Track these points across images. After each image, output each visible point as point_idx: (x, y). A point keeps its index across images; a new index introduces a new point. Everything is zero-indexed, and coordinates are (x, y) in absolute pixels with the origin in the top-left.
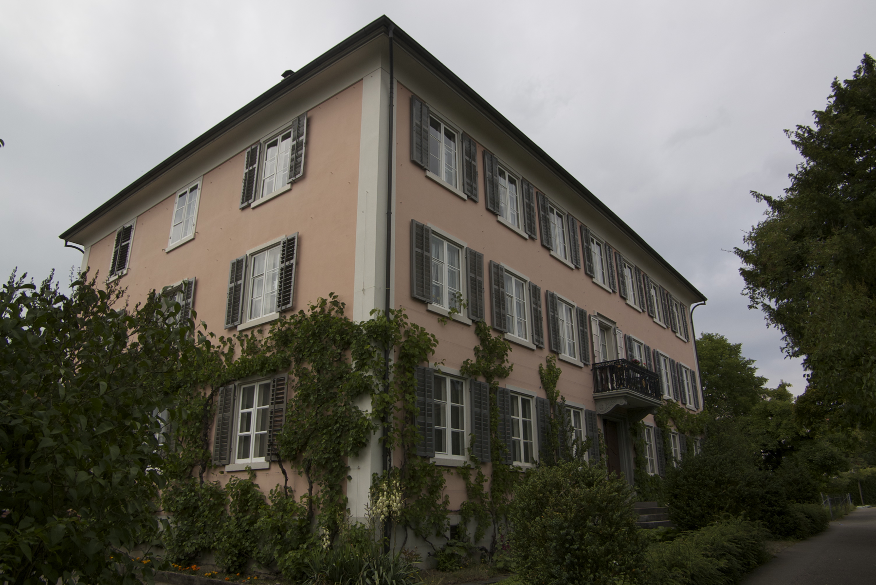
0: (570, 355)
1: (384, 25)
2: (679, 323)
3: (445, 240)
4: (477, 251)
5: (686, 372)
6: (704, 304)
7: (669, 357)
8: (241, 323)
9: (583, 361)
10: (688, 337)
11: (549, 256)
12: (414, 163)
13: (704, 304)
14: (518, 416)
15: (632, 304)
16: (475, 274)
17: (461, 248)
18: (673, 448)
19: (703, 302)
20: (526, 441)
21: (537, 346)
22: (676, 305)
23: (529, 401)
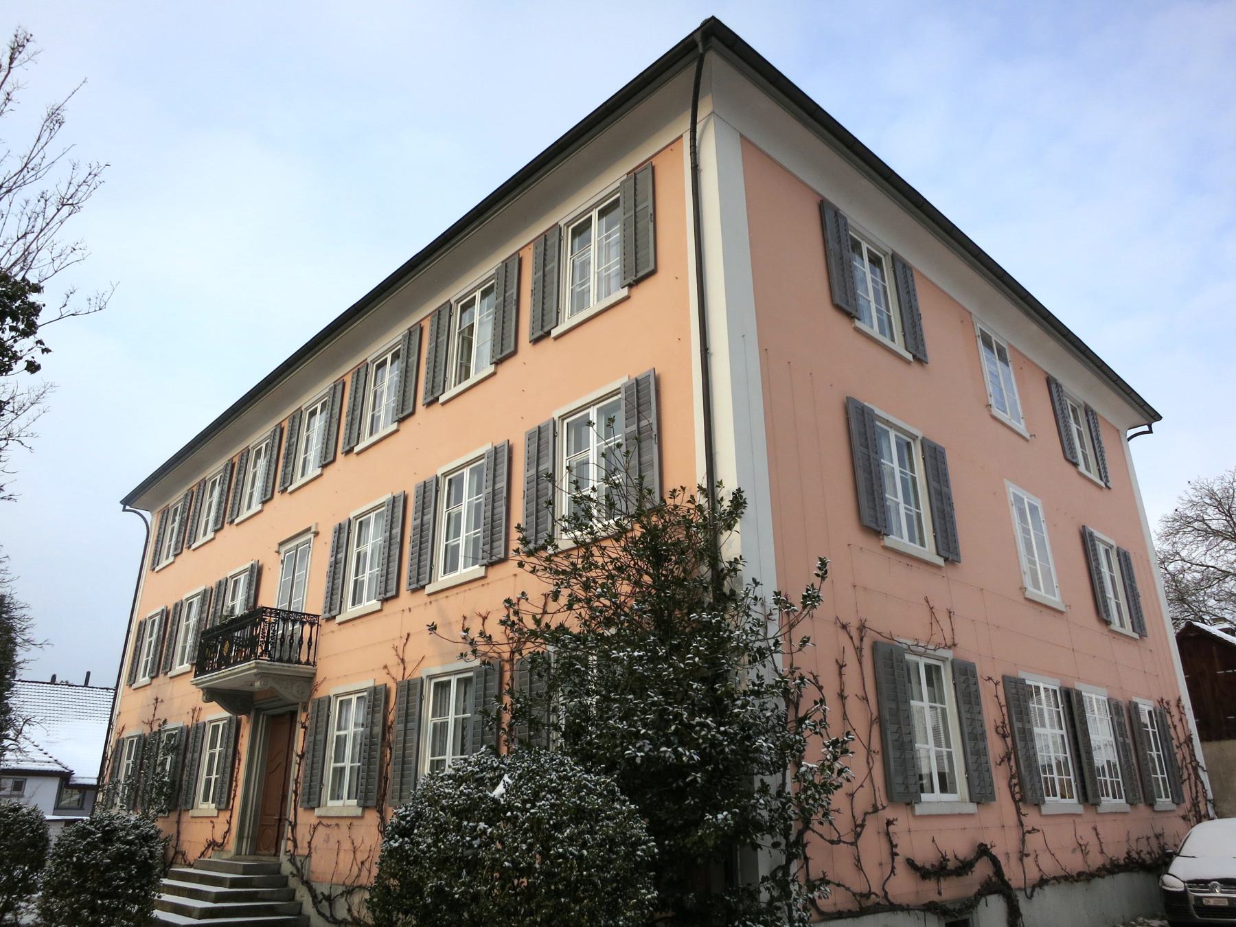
0: (912, 539)
1: (713, 18)
2: (1082, 446)
3: (891, 427)
4: (939, 443)
5: (1107, 552)
6: (1150, 431)
7: (920, 434)
8: (430, 582)
9: (942, 553)
10: (1106, 477)
11: (1076, 474)
12: (838, 308)
13: (1150, 431)
14: (922, 700)
15: (875, 332)
16: (939, 483)
17: (914, 440)
18: (190, 641)
19: (1146, 428)
20: (937, 749)
21: (946, 560)
22: (1074, 410)
23: (938, 668)
